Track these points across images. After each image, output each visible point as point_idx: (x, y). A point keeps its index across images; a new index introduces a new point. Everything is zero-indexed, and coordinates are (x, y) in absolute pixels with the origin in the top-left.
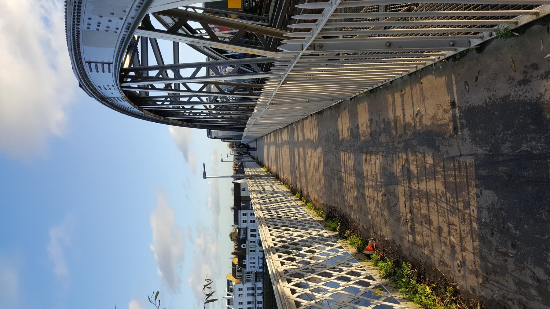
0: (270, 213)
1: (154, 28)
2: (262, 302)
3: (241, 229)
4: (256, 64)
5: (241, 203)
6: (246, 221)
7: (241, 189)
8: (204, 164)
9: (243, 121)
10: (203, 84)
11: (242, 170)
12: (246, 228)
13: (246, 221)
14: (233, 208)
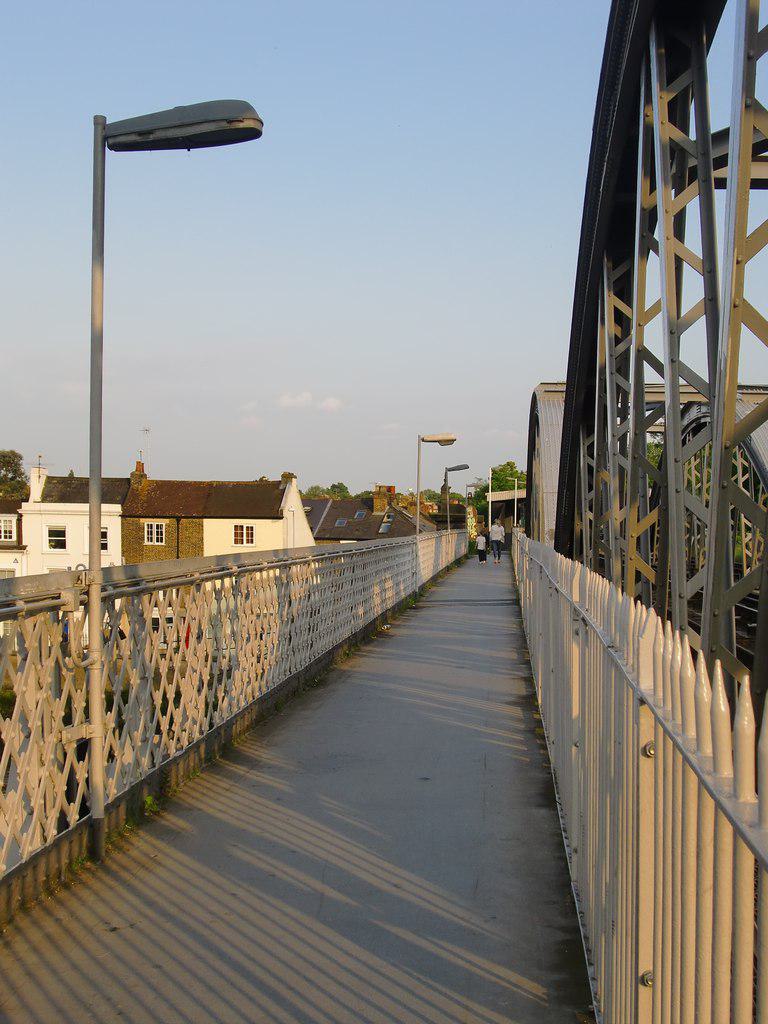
0: (221, 673)
1: (749, 258)
2: (244, 548)
3: (14, 518)
4: (702, 589)
5: (164, 522)
6: (61, 545)
7: (245, 523)
8: (467, 467)
9: (588, 552)
10: (743, 328)
11: (377, 533)
12: (20, 546)
13: (61, 545)
14: (261, 480)
